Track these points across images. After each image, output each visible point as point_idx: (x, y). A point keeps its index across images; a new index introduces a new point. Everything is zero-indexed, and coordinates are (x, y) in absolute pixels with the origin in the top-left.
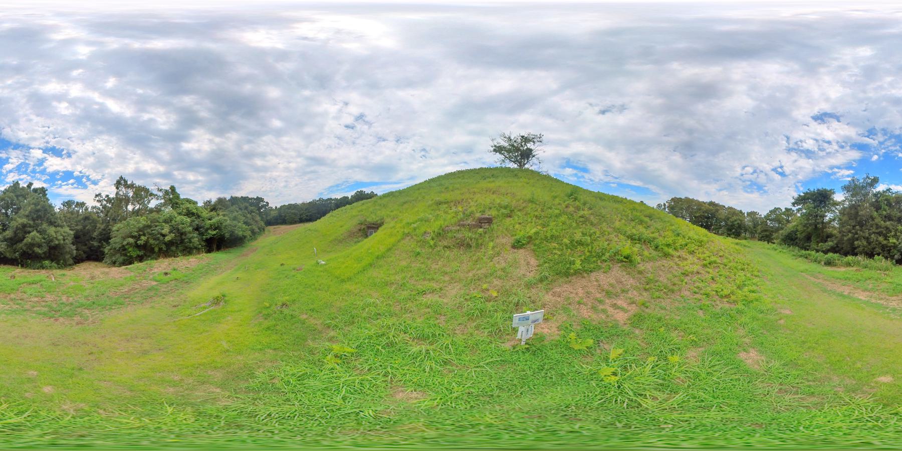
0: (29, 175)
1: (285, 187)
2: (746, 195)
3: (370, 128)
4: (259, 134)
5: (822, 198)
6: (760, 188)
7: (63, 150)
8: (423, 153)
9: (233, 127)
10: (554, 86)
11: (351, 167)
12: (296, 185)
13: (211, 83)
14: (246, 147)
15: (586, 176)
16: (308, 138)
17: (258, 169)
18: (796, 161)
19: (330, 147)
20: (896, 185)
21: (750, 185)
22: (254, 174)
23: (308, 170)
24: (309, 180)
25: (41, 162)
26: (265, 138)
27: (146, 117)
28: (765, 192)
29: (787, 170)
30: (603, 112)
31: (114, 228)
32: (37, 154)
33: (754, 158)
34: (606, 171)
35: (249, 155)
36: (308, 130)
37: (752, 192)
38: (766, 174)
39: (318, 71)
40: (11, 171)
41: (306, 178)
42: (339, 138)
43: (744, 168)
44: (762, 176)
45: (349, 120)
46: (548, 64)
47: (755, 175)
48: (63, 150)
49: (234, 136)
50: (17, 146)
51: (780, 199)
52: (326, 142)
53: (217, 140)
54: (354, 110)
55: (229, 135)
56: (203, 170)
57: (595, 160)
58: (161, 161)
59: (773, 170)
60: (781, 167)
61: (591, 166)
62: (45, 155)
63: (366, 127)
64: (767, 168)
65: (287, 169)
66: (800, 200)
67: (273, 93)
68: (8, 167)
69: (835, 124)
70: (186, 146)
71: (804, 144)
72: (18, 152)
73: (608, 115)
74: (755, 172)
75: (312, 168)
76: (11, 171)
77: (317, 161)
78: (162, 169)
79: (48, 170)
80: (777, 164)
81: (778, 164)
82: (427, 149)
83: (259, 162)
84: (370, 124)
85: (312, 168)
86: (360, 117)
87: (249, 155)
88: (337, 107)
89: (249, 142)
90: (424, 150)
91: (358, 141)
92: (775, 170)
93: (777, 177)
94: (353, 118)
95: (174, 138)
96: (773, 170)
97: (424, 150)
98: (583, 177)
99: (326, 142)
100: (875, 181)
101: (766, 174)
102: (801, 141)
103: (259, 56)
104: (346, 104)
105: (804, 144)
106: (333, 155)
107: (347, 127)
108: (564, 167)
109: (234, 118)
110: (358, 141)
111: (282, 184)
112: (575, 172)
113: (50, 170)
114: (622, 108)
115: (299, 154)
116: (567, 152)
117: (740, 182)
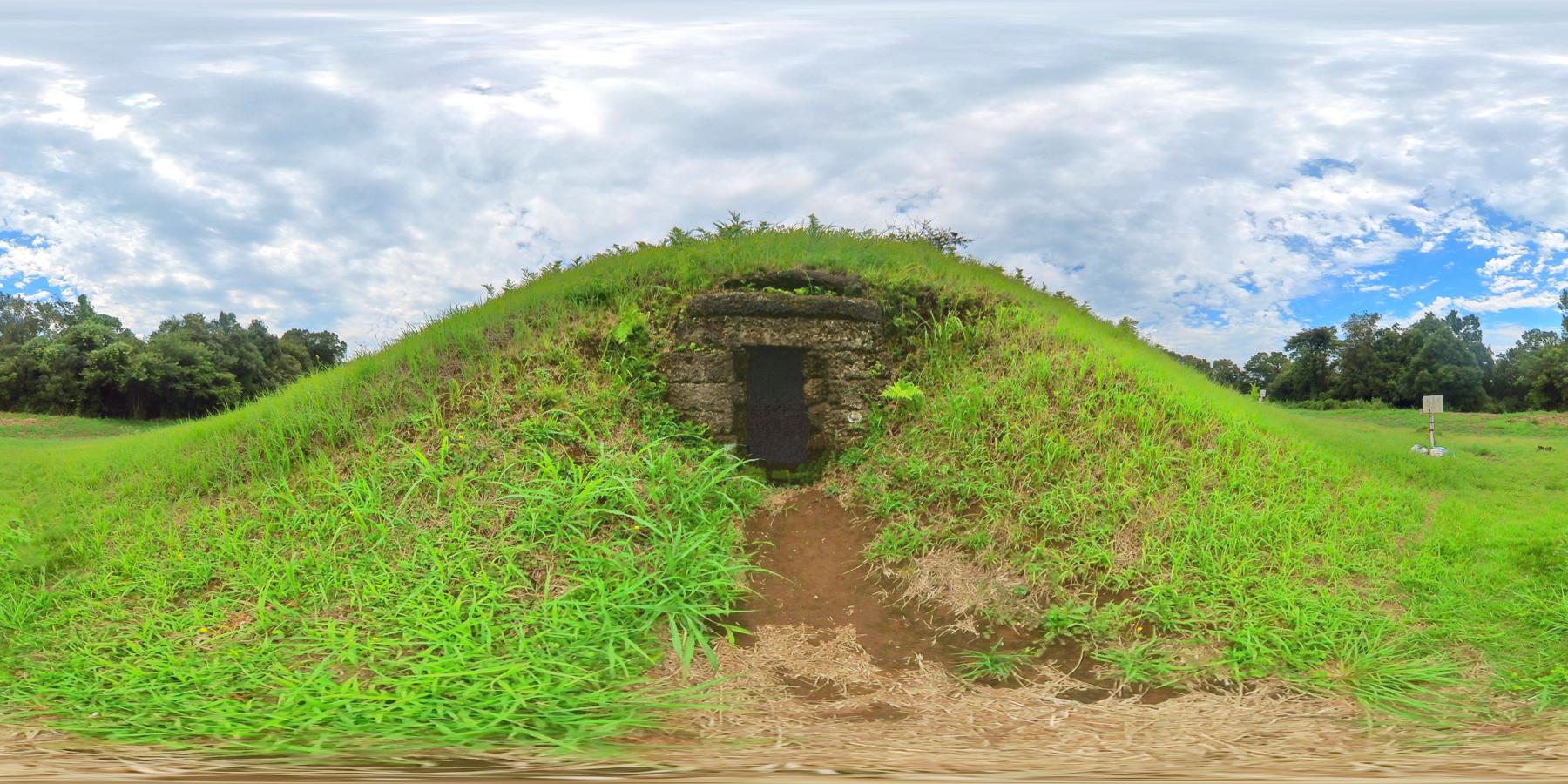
2: (1189, 330)
5: (1320, 338)
6: (1214, 315)
13: (339, 157)
14: (356, 264)
20: (1467, 297)
21: (1196, 312)
26: (390, 251)
27: (216, 194)
28: (1225, 323)
29: (1261, 279)
35: (360, 278)
37: (1200, 325)
45: (525, 237)
49: (342, 243)
51: (1270, 334)
53: (314, 247)
54: (533, 222)
56: (280, 292)
58: (210, 272)
66: (1295, 342)
67: (426, 187)
69: (1340, 178)
70: (264, 251)
78: (208, 284)
81: (1242, 269)
87: (360, 278)
88: (511, 217)
89: (362, 255)
92: (1237, 281)
93: (1244, 293)
94: (530, 233)
95: (245, 233)
100: (1375, 317)
104: (524, 212)
107: (521, 245)
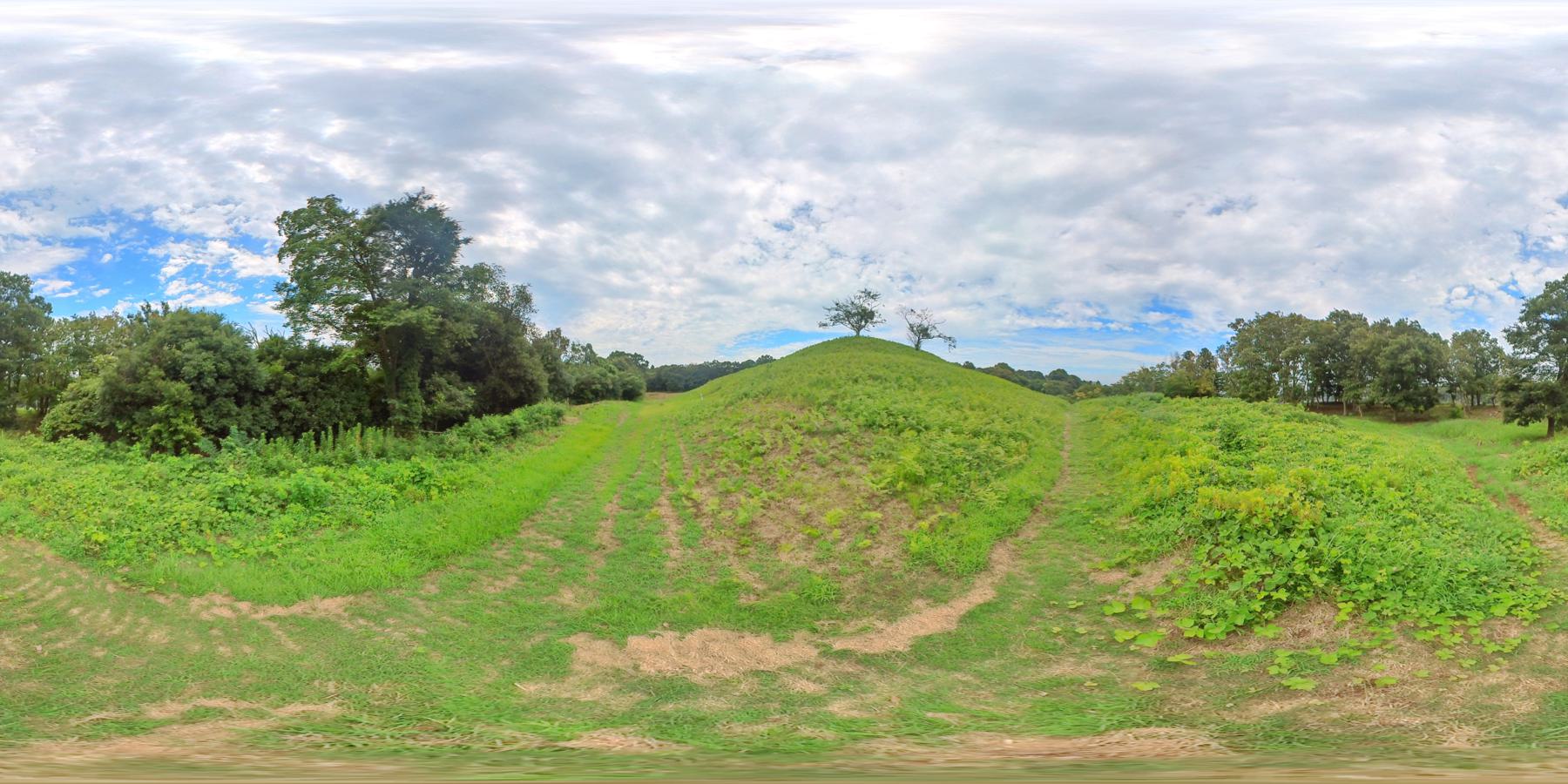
0: (205, 284)
1: (661, 328)
3: (818, 230)
4: (620, 228)
7: (265, 241)
8: (906, 284)
9: (576, 213)
10: (1143, 163)
11: (778, 302)
12: (680, 326)
14: (595, 250)
15: (1186, 323)
16: (709, 244)
17: (615, 293)
18: (1539, 271)
19: (743, 261)
22: (606, 300)
23: (703, 300)
24: (703, 318)
25: (224, 263)
30: (1218, 211)
31: (352, 344)
32: (219, 248)
33: (1468, 273)
34: (1219, 313)
36: (708, 226)
38: (1490, 297)
39: (732, 117)
40: (173, 278)
41: (698, 315)
42: (763, 246)
43: (1450, 291)
44: (1484, 301)
46: (1132, 126)
47: (1472, 298)
48: (265, 241)
49: (571, 231)
50: (179, 238)
52: (737, 250)
53: (542, 234)
54: (793, 194)
55: (566, 226)
57: (1202, 294)
59: (1501, 289)
60: (1514, 283)
61: (1194, 306)
62: (233, 250)
63: (812, 228)
64: (1491, 286)
65: (664, 296)
67: (647, 152)
68: (170, 270)
71: (1551, 245)
72: (184, 246)
73: (1226, 215)
74: (1470, 294)
75: (710, 299)
76: (173, 278)
77: (719, 286)
79: (239, 276)
80: (1506, 278)
82: (915, 276)
83: (616, 279)
84: (818, 224)
85: (710, 299)
86: (804, 210)
87: (599, 265)
90: (909, 277)
91: (794, 254)
92: (1504, 288)
96: (1501, 289)
97: (909, 277)
98: (1179, 325)
99: (737, 250)
101: (1490, 297)
102: (1544, 239)
103: (631, 84)
105: (1551, 245)
106: (750, 277)
107: (779, 226)
108: (1147, 310)
109: (580, 196)
110: (794, 254)
111: (656, 324)
112: (1166, 317)
113: (243, 274)
114: (1249, 205)
115: (689, 272)
116: (1153, 283)
117: (1446, 313)
